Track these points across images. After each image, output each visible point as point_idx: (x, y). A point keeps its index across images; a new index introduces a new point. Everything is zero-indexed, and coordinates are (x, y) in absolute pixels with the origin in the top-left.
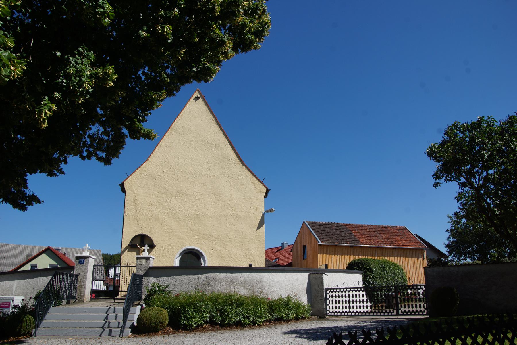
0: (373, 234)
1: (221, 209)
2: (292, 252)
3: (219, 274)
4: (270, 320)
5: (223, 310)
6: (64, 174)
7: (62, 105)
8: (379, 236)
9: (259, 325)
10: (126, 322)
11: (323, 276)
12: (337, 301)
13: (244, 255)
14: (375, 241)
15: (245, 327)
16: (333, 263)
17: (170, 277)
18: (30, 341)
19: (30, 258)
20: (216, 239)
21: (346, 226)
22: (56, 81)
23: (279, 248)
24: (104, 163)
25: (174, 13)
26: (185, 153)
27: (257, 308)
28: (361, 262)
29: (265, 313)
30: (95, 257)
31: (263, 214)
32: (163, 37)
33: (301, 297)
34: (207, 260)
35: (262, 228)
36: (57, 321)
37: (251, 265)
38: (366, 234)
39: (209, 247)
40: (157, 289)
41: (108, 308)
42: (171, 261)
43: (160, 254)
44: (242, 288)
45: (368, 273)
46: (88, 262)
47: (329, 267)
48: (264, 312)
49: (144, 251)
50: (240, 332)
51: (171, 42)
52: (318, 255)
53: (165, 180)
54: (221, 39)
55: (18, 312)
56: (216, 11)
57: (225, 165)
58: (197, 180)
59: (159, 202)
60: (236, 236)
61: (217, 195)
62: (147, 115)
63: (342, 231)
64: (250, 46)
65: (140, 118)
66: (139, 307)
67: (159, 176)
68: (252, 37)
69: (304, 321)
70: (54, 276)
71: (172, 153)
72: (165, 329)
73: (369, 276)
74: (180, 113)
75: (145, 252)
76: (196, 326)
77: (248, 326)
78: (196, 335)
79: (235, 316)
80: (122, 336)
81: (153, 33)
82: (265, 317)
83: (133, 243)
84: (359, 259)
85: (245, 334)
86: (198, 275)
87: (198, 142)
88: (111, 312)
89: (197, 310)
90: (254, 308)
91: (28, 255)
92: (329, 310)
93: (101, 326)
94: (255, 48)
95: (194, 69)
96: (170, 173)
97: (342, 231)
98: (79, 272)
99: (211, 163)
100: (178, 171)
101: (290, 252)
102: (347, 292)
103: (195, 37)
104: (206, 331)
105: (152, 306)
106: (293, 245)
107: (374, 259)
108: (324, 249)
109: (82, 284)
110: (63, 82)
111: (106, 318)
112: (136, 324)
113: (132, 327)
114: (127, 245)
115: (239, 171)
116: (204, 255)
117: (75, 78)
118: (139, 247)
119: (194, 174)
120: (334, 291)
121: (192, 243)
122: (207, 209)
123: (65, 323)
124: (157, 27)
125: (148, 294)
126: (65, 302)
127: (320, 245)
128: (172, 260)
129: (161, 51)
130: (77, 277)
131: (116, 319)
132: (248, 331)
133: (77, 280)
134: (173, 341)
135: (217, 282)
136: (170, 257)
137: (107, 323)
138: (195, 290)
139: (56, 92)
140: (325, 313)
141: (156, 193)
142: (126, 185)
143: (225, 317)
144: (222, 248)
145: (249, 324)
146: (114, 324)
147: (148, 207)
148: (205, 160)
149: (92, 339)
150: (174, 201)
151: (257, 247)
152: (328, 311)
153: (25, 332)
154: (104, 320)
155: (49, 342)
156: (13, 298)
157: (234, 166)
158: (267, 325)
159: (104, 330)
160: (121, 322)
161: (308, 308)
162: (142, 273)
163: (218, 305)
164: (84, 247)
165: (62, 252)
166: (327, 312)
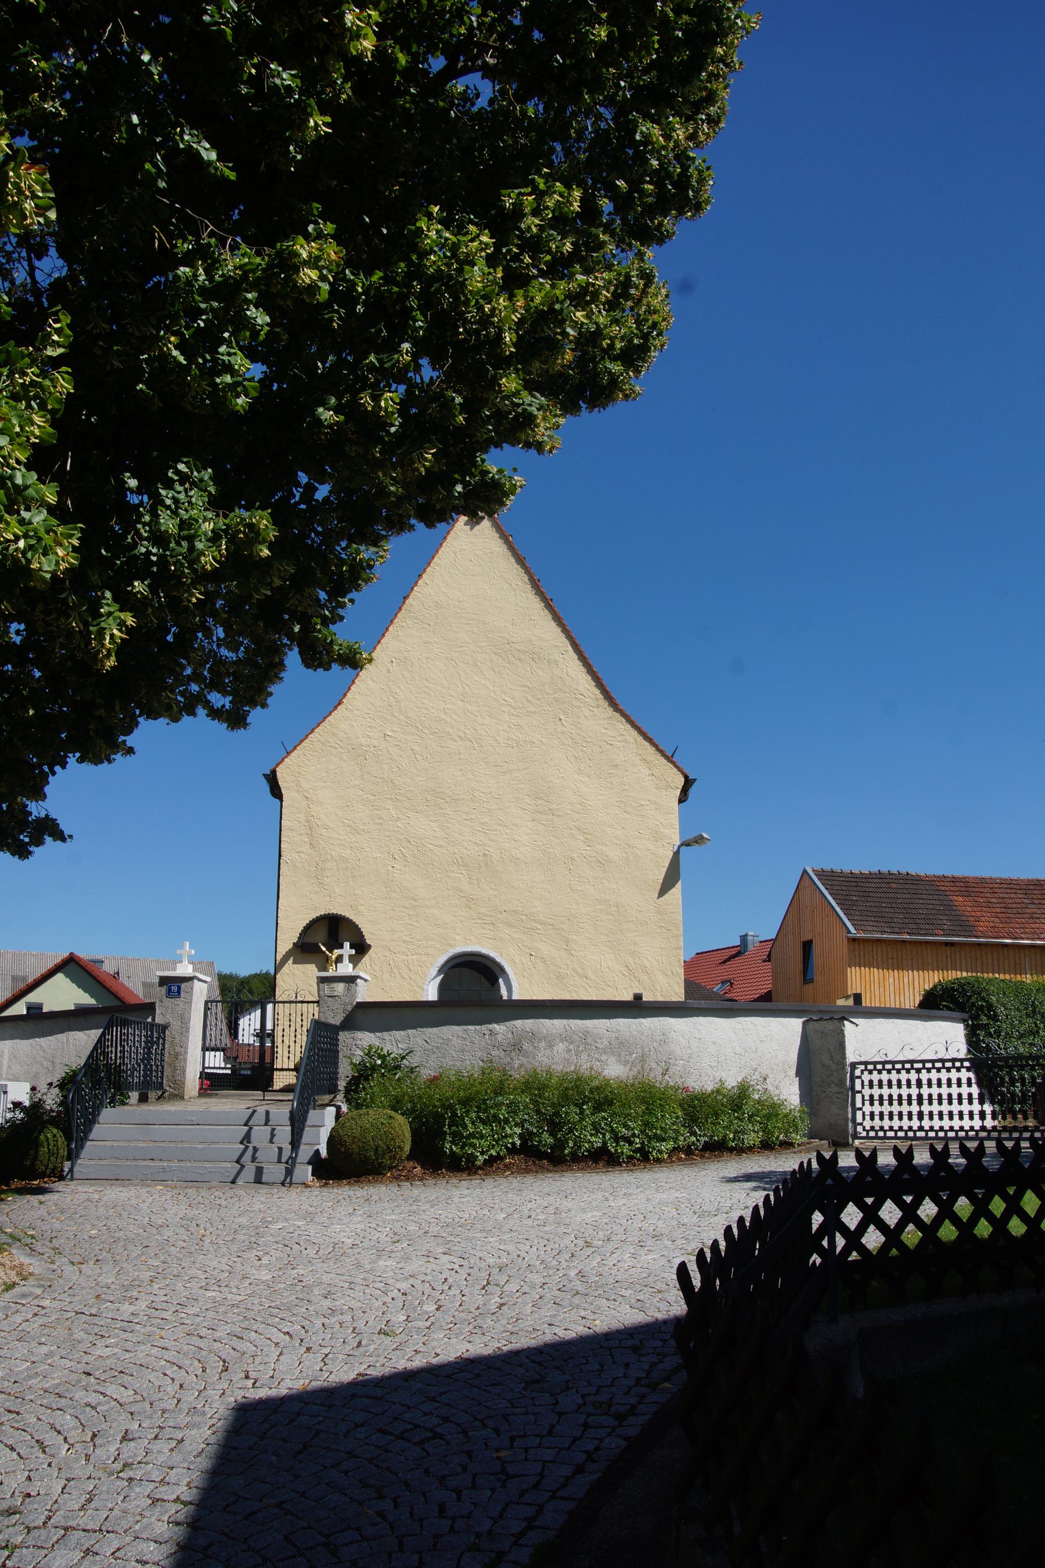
0: (1019, 906)
1: (553, 838)
2: (769, 961)
3: (547, 1020)
4: (689, 1147)
5: (557, 1117)
6: (134, 754)
7: (150, 611)
8: (1035, 911)
9: (658, 1161)
10: (298, 1147)
11: (844, 1025)
12: (895, 1103)
14: (1022, 926)
15: (620, 1164)
16: (892, 995)
17: (414, 1031)
18: (60, 1189)
19: (22, 986)
20: (541, 923)
21: (934, 883)
22: (133, 553)
23: (733, 952)
24: (226, 725)
25: (401, 359)
26: (446, 679)
27: (652, 1113)
28: (963, 988)
29: (675, 1127)
30: (208, 979)
31: (675, 850)
32: (376, 422)
33: (781, 1085)
34: (517, 985)
35: (674, 889)
36: (121, 1144)
37: (638, 997)
38: (994, 905)
40: (379, 1062)
41: (250, 1111)
44: (612, 1059)
45: (981, 1020)
46: (190, 992)
47: (866, 1002)
48: (673, 1124)
49: (339, 959)
50: (604, 1177)
51: (397, 430)
52: (849, 969)
54: (523, 409)
55: (23, 1119)
56: (505, 343)
59: (379, 821)
60: (598, 914)
62: (343, 606)
63: (920, 896)
64: (612, 393)
65: (327, 613)
66: (331, 1111)
68: (616, 367)
69: (789, 1151)
70: (108, 1028)
72: (401, 1168)
73: (986, 1027)
74: (429, 563)
75: (342, 962)
76: (485, 1159)
77: (628, 1162)
78: (484, 1184)
79: (591, 1135)
80: (291, 1184)
81: (350, 410)
82: (676, 1140)
83: (308, 940)
84: (958, 979)
85: (618, 1181)
86: (490, 1023)
87: (481, 647)
88: (257, 1122)
89: (487, 1117)
90: (644, 1112)
91: (14, 979)
92: (861, 1124)
93: (235, 1158)
94: (626, 397)
95: (459, 488)
96: (405, 739)
97: (920, 896)
98: (169, 1018)
100: (428, 732)
101: (764, 962)
102: (913, 1072)
103: (457, 413)
104: (512, 1173)
105: (367, 1107)
106: (774, 940)
107: (1003, 981)
108: (866, 952)
109: (178, 1049)
110: (149, 553)
111: (247, 1137)
112: (324, 1153)
113: (316, 1161)
114: (291, 946)
116: (507, 970)
117: (178, 544)
118: (324, 949)
120: (875, 1069)
121: (472, 938)
123: (143, 1147)
124: (362, 399)
125: (353, 1076)
126: (134, 1096)
127: (854, 940)
129: (375, 456)
130: (164, 1033)
131: (271, 1142)
132: (626, 1175)
133: (164, 1040)
134: (423, 1196)
135: (543, 1044)
136: (413, 977)
137: (250, 1151)
138: (481, 1063)
139: (137, 580)
140: (851, 1131)
143: (564, 1137)
145: (630, 1158)
146: (268, 1153)
148: (504, 698)
149: (214, 1190)
152: (858, 1127)
153: (46, 1169)
154: (242, 1143)
155: (107, 1192)
156: (6, 1085)
157: (588, 713)
158: (680, 1159)
159: (243, 1166)
160: (287, 1148)
161: (800, 1116)
162: (336, 1020)
163: (543, 1104)
164: (178, 952)
165: (108, 968)
166: (855, 1129)
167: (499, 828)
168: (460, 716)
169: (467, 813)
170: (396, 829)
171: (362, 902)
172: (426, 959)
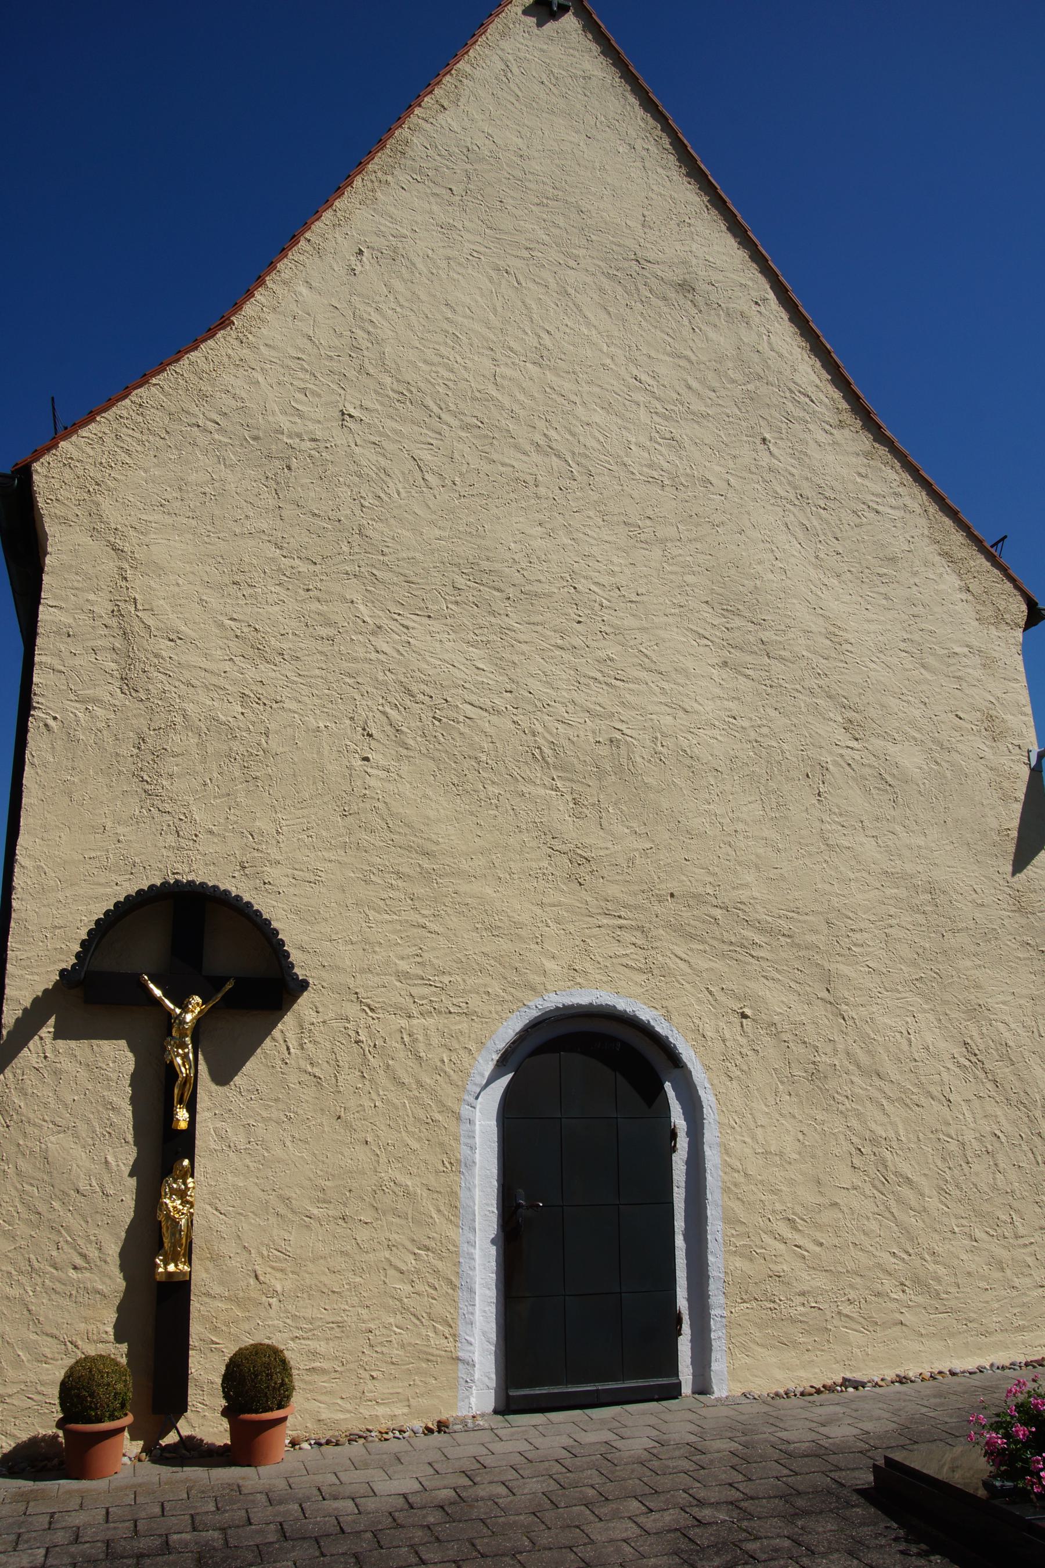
13: (958, 1051)
20: (762, 931)
34: (712, 1099)
39: (721, 997)
42: (438, 1116)
43: (344, 1059)
53: (360, 476)
57: (763, 423)
58: (595, 496)
59: (324, 632)
60: (893, 911)
61: (738, 613)
67: (309, 444)
71: (406, 304)
99: (675, 396)
100: (455, 423)
115: (860, 474)
118: (158, 993)
119: (574, 453)
121: (589, 966)
128: (444, 1108)
141: (297, 562)
142: (52, 490)
144: (809, 1004)
147: (227, 666)
151: (1025, 992)
157: (822, 437)
167: (643, 675)
168: (533, 398)
169: (563, 633)
170: (374, 656)
171: (274, 854)
172: (464, 1026)
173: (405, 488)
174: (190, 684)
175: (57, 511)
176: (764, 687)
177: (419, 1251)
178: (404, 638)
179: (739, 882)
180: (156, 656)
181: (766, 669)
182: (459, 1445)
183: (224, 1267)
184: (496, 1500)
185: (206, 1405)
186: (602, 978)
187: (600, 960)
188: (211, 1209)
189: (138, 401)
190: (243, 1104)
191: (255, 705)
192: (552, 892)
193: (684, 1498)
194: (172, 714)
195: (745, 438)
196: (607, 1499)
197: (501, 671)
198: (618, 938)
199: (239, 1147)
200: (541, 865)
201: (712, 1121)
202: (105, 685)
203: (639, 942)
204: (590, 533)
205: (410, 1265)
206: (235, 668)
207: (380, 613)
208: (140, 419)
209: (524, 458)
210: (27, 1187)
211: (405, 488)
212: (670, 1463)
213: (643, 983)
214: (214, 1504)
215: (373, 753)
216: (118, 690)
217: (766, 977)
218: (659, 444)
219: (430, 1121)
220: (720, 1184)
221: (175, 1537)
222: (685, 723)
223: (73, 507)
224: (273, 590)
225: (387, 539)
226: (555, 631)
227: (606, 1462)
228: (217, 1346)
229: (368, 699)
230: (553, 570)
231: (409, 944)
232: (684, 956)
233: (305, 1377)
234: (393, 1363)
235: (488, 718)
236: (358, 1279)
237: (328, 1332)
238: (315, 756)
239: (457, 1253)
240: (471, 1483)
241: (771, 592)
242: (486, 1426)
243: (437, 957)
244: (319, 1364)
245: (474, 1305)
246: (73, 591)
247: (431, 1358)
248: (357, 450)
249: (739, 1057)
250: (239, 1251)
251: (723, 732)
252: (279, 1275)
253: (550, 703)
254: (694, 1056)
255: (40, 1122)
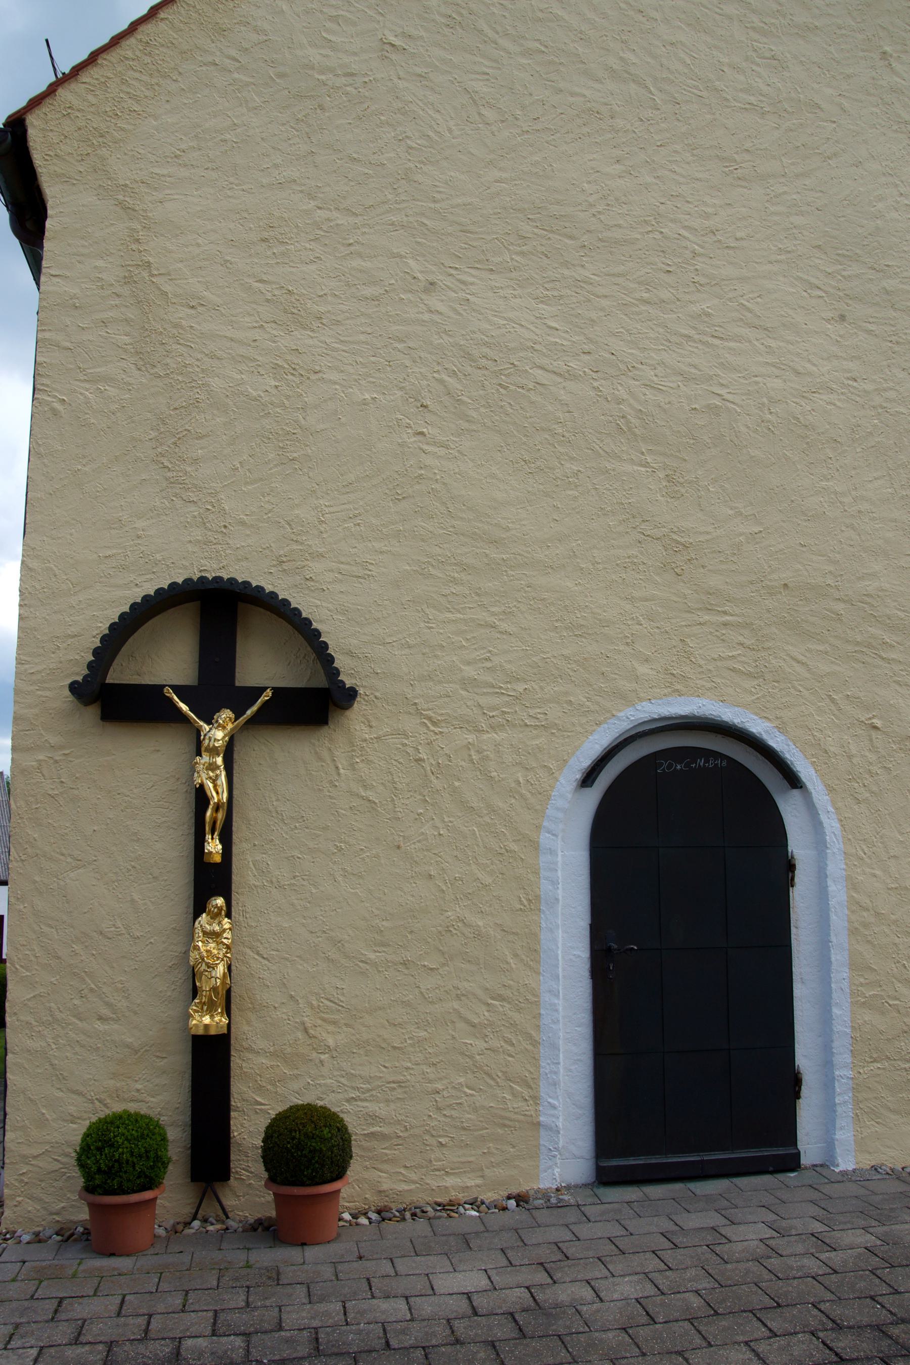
34: (836, 824)
42: (514, 847)
59: (368, 291)
122: (798, 373)
141: (335, 214)
150: (502, 293)
170: (426, 317)
173: (458, 125)
174: (213, 356)
175: (56, 169)
176: (890, 345)
177: (492, 1002)
178: (461, 295)
179: (865, 571)
180: (176, 326)
181: (892, 322)
182: (539, 1226)
183: (268, 1019)
184: (579, 1307)
185: (251, 1173)
186: (705, 683)
187: (702, 662)
188: (251, 954)
189: (145, 39)
190: (286, 833)
191: (290, 377)
192: (644, 584)
193: (816, 1316)
194: (196, 391)
195: (861, 54)
196: (716, 1313)
197: (577, 329)
198: (723, 637)
199: (282, 883)
200: (630, 552)
201: (835, 850)
202: (119, 361)
203: (748, 642)
204: (677, 169)
205: (482, 1018)
206: (266, 336)
207: (433, 268)
208: (148, 60)
209: (597, 86)
210: (45, 929)
211: (458, 125)
212: (791, 1261)
213: (753, 689)
214: (244, 1298)
215: (429, 427)
216: (133, 367)
217: (898, 683)
218: (758, 65)
219: (503, 851)
220: (846, 924)
221: (189, 1342)
222: (798, 387)
223: (76, 163)
224: (308, 246)
225: (437, 184)
226: (639, 283)
227: (715, 1257)
228: (263, 1107)
229: (421, 366)
230: (635, 213)
231: (476, 646)
232: (801, 658)
233: (363, 1143)
234: (464, 1129)
235: (564, 384)
236: (423, 1034)
237: (389, 1092)
238: (361, 432)
239: (537, 1004)
240: (549, 1281)
241: (895, 233)
242: (572, 1201)
243: (510, 662)
244: (378, 1129)
245: (559, 1063)
246: (78, 258)
247: (507, 1122)
248: (401, 84)
249: (867, 776)
250: (284, 1001)
251: (842, 397)
252: (331, 1028)
253: (636, 365)
254: (814, 774)
255: (57, 856)
